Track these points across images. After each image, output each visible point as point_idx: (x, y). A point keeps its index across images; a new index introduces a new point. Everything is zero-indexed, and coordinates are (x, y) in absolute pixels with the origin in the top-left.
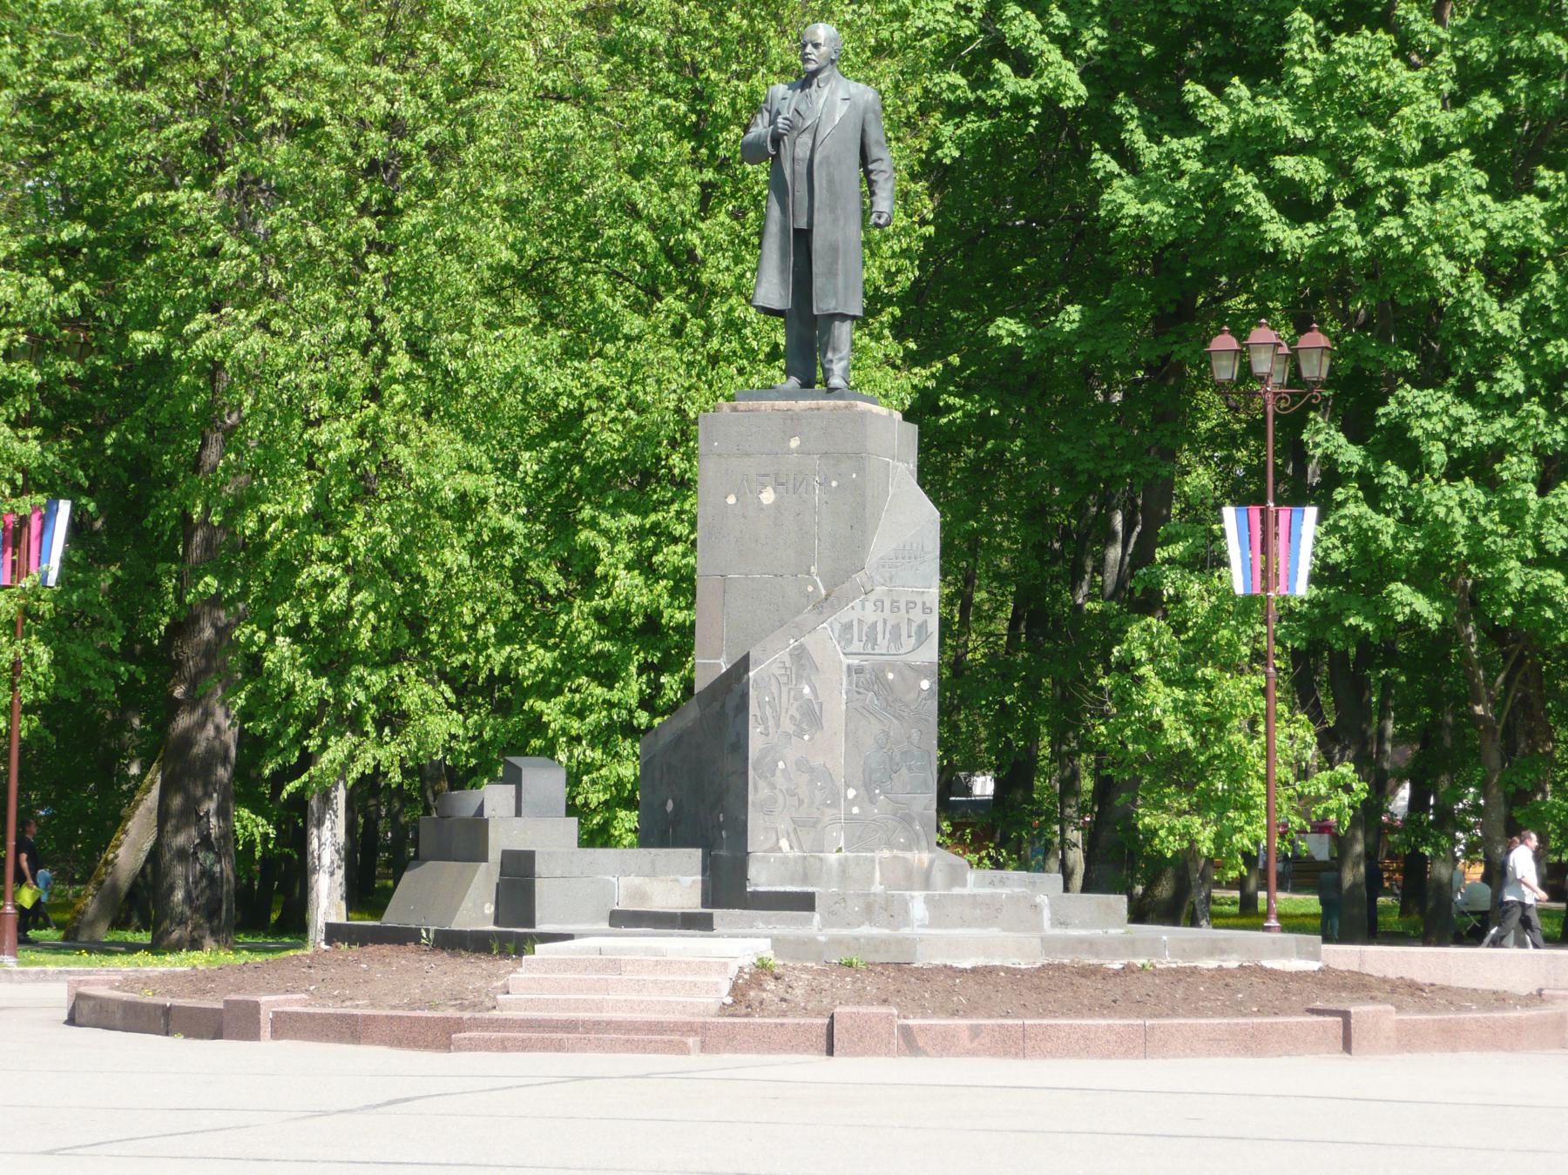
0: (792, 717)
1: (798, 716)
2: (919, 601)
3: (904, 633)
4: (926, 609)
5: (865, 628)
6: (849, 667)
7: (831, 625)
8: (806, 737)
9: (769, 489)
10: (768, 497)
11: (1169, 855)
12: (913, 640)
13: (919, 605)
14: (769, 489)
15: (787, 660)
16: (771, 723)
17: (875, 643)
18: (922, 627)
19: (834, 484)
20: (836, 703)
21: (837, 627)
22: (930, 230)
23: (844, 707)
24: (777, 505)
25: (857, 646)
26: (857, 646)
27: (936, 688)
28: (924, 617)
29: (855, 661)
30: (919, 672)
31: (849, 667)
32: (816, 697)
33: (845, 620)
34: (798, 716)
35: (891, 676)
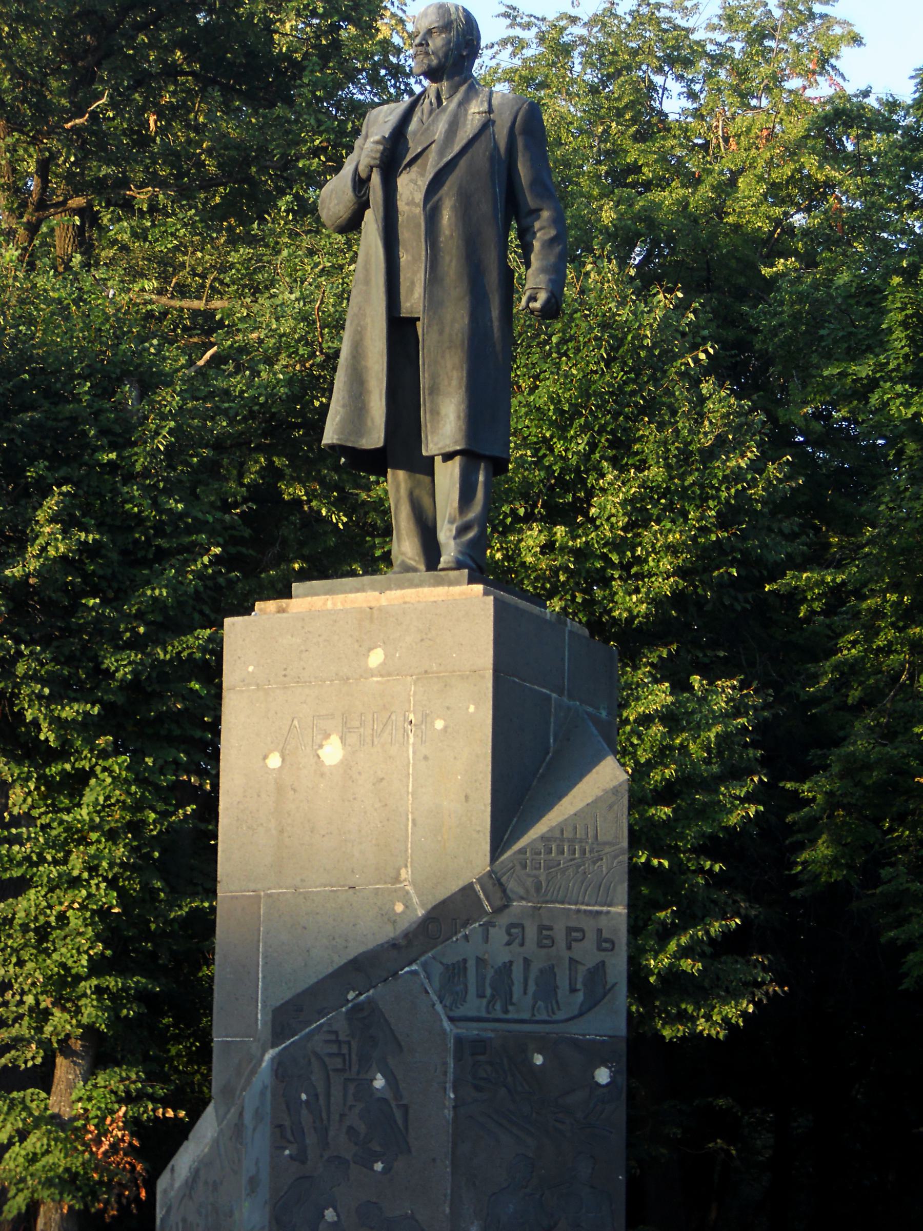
0: (351, 1130)
1: (362, 1128)
2: (589, 925)
3: (563, 982)
4: (605, 943)
5: (490, 973)
6: (459, 1040)
7: (424, 966)
8: (379, 1166)
9: (335, 739)
10: (332, 752)
11: (198, 16)
12: (580, 996)
13: (591, 936)
14: (335, 739)
15: (342, 1026)
16: (311, 1140)
17: (508, 1000)
18: (598, 971)
19: (439, 724)
20: (437, 1108)
21: (437, 970)
22: (748, 606)
23: (449, 1113)
24: (346, 765)
25: (473, 1006)
26: (473, 1006)
27: (622, 1080)
28: (601, 956)
29: (472, 1031)
30: (596, 1054)
31: (459, 1040)
32: (398, 1095)
33: (451, 958)
34: (362, 1128)
35: (539, 1060)
